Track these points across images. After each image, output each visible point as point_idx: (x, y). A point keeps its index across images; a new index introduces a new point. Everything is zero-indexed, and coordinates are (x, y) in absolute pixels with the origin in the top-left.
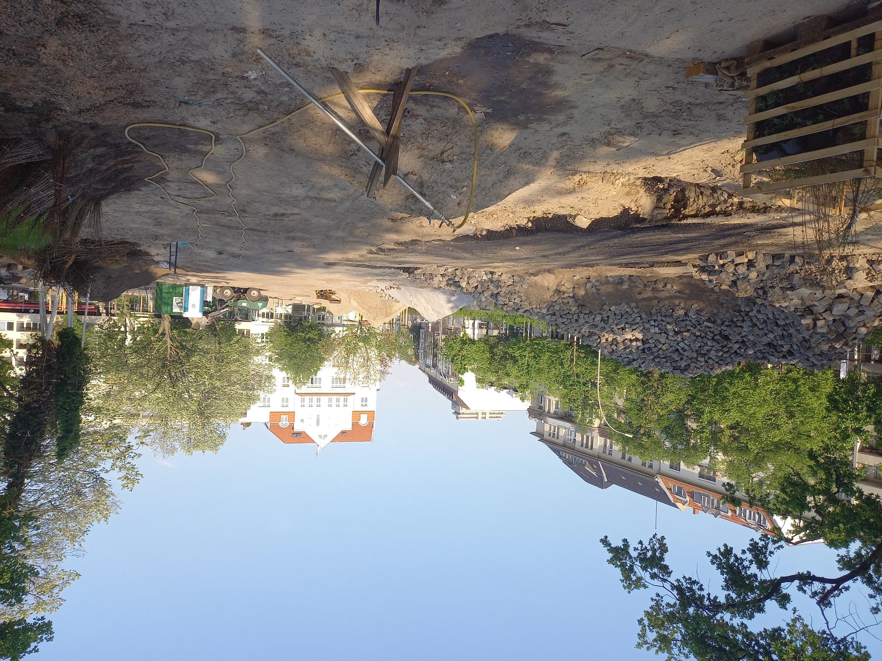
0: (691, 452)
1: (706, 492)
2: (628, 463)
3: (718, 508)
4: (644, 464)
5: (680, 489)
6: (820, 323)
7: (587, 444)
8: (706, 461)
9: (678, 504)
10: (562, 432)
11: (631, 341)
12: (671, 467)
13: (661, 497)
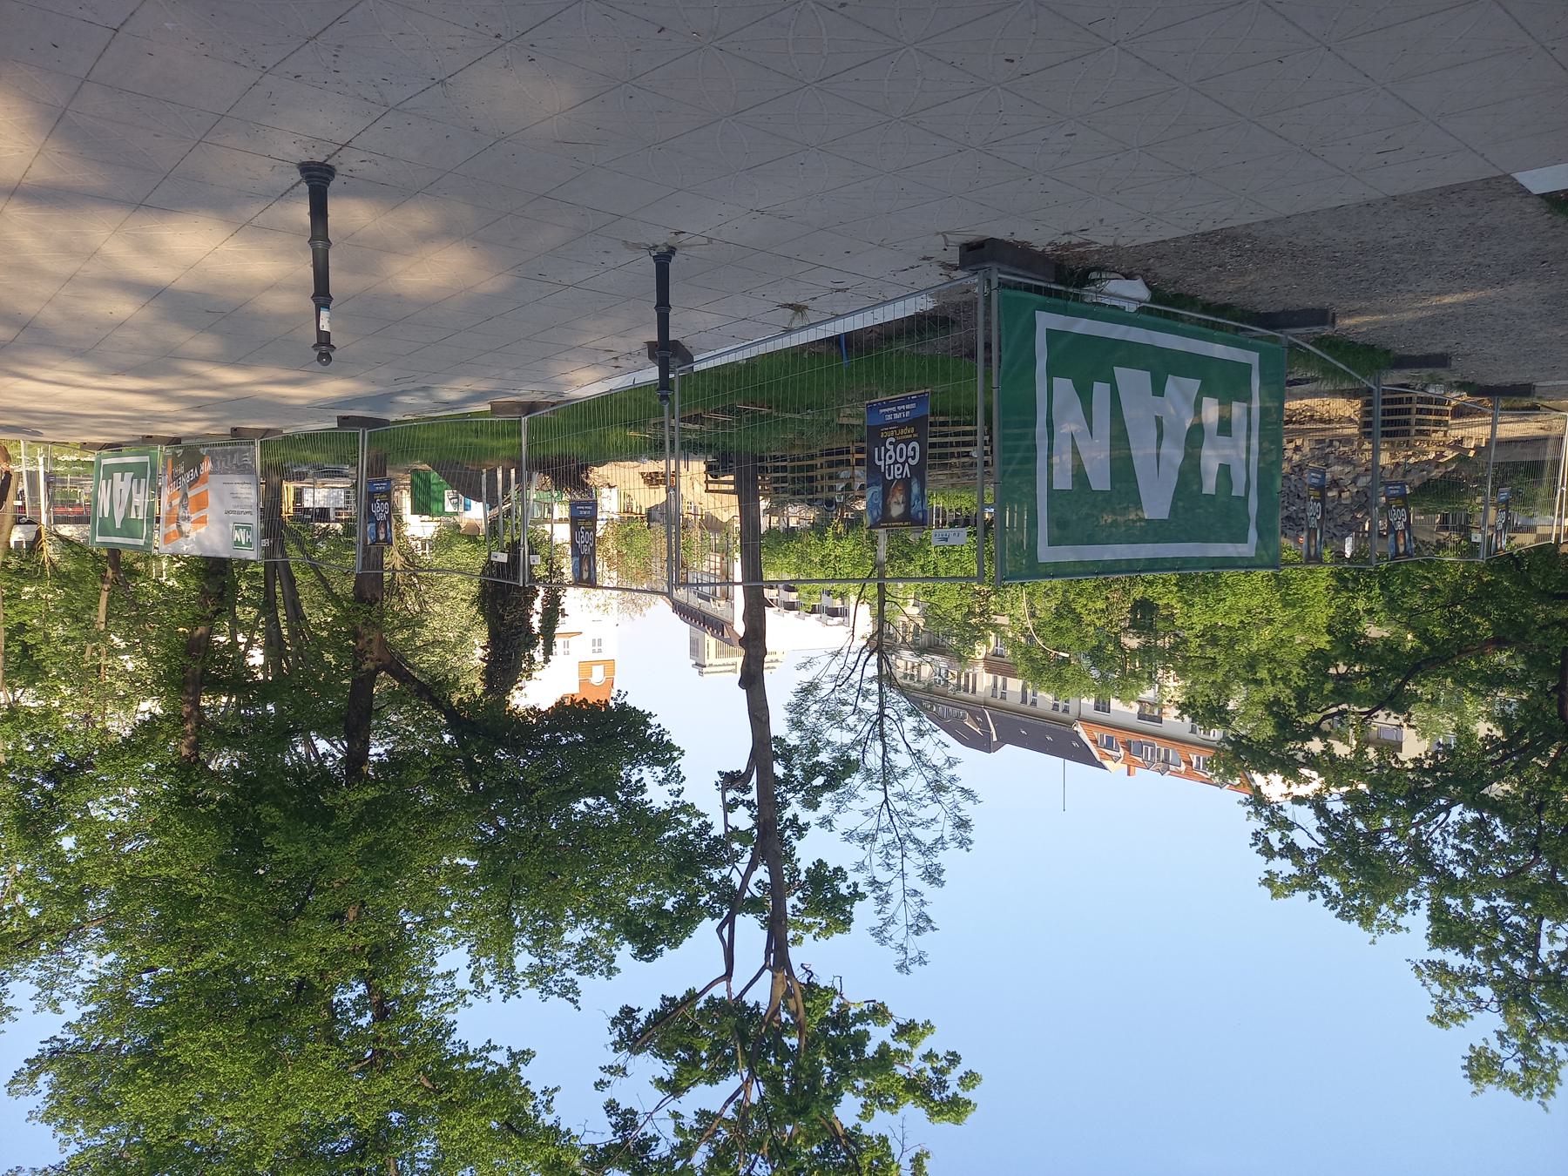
0: (1127, 683)
1: (1149, 740)
2: (1032, 708)
3: (1166, 761)
4: (1056, 707)
5: (1110, 739)
6: (1344, 495)
7: (967, 685)
8: (1149, 694)
9: (1105, 763)
10: (926, 671)
11: (1134, 521)
12: (1097, 708)
13: (1084, 756)
